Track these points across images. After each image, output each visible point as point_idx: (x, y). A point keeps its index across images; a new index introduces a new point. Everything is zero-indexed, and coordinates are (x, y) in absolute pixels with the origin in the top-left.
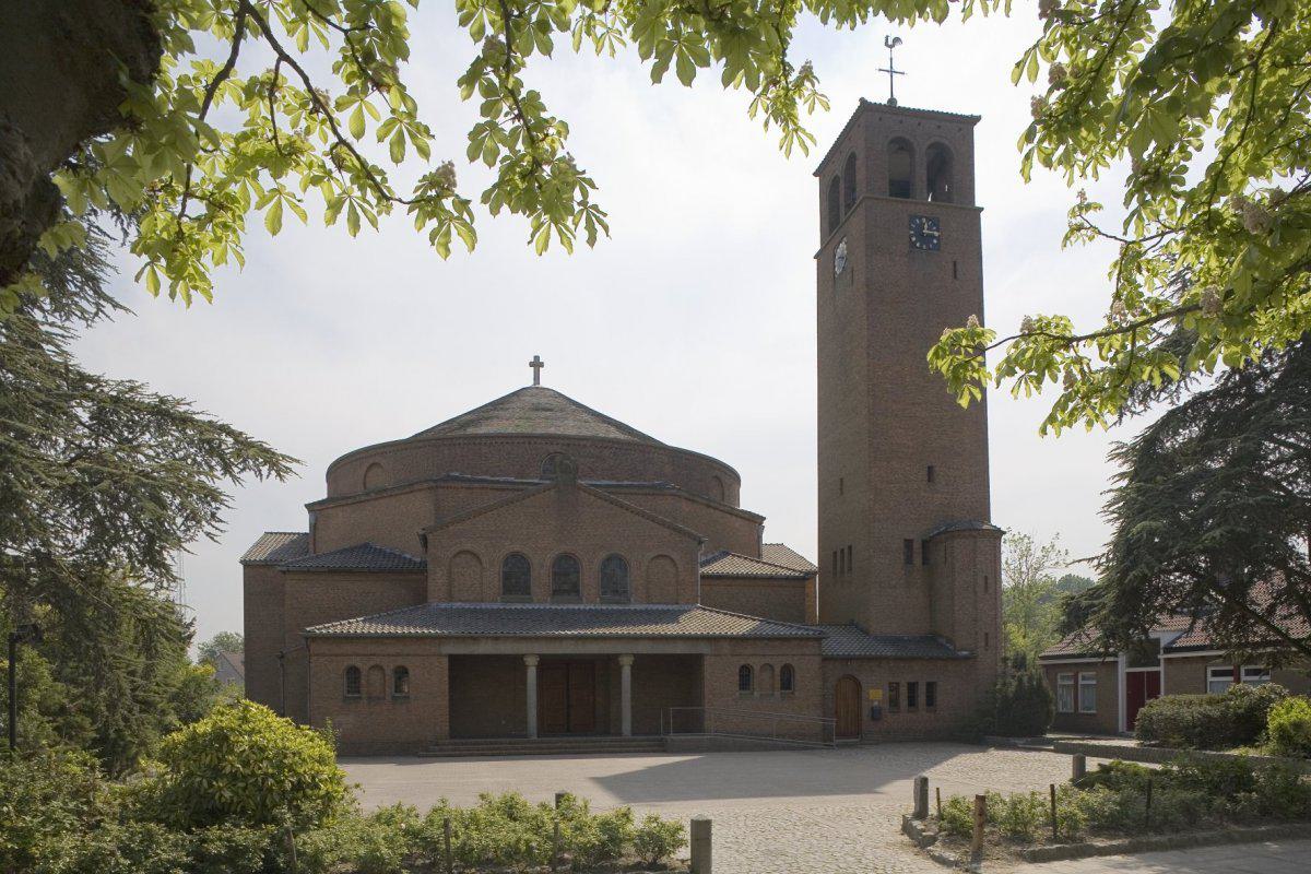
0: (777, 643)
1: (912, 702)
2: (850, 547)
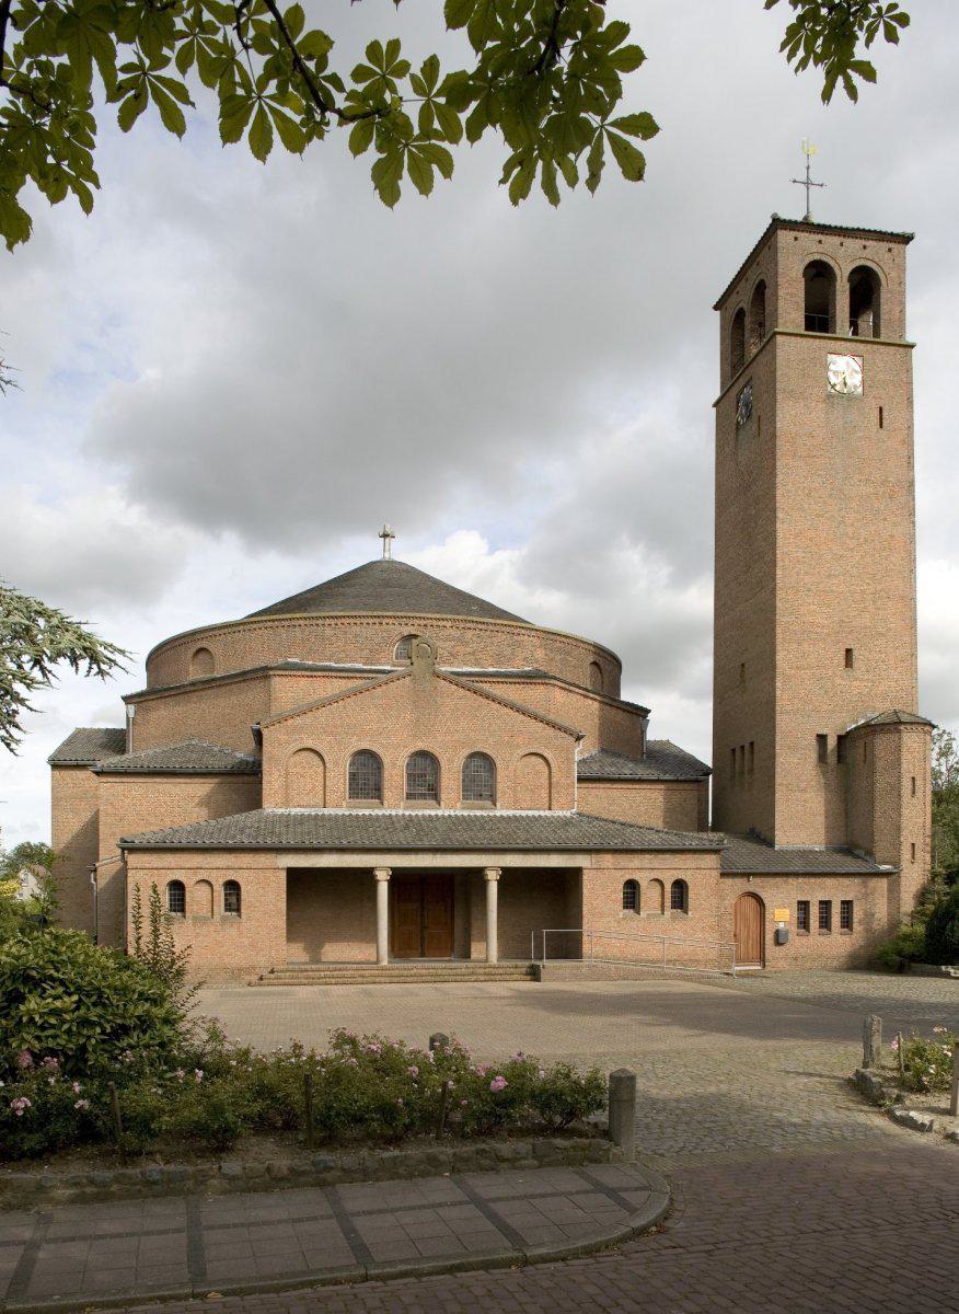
1: (825, 923)
2: (752, 744)
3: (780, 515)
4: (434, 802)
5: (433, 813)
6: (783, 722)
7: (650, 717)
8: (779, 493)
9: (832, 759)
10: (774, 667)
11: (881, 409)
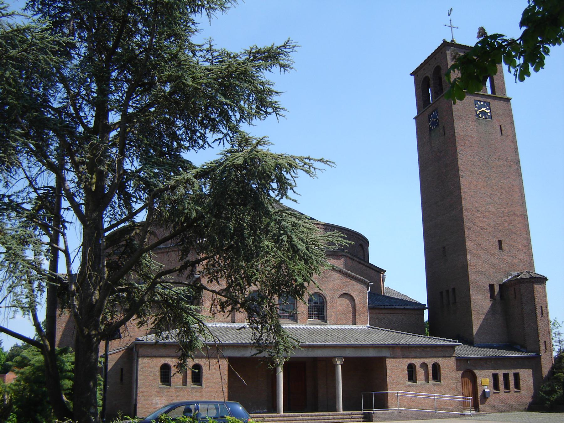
0: (429, 349)
1: (507, 386)
2: (454, 289)
3: (461, 173)
4: (292, 320)
5: (294, 326)
6: (472, 278)
7: (386, 274)
8: (459, 163)
9: (498, 298)
10: (465, 250)
11: (500, 126)
